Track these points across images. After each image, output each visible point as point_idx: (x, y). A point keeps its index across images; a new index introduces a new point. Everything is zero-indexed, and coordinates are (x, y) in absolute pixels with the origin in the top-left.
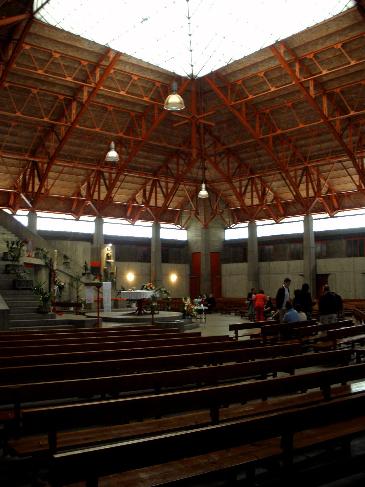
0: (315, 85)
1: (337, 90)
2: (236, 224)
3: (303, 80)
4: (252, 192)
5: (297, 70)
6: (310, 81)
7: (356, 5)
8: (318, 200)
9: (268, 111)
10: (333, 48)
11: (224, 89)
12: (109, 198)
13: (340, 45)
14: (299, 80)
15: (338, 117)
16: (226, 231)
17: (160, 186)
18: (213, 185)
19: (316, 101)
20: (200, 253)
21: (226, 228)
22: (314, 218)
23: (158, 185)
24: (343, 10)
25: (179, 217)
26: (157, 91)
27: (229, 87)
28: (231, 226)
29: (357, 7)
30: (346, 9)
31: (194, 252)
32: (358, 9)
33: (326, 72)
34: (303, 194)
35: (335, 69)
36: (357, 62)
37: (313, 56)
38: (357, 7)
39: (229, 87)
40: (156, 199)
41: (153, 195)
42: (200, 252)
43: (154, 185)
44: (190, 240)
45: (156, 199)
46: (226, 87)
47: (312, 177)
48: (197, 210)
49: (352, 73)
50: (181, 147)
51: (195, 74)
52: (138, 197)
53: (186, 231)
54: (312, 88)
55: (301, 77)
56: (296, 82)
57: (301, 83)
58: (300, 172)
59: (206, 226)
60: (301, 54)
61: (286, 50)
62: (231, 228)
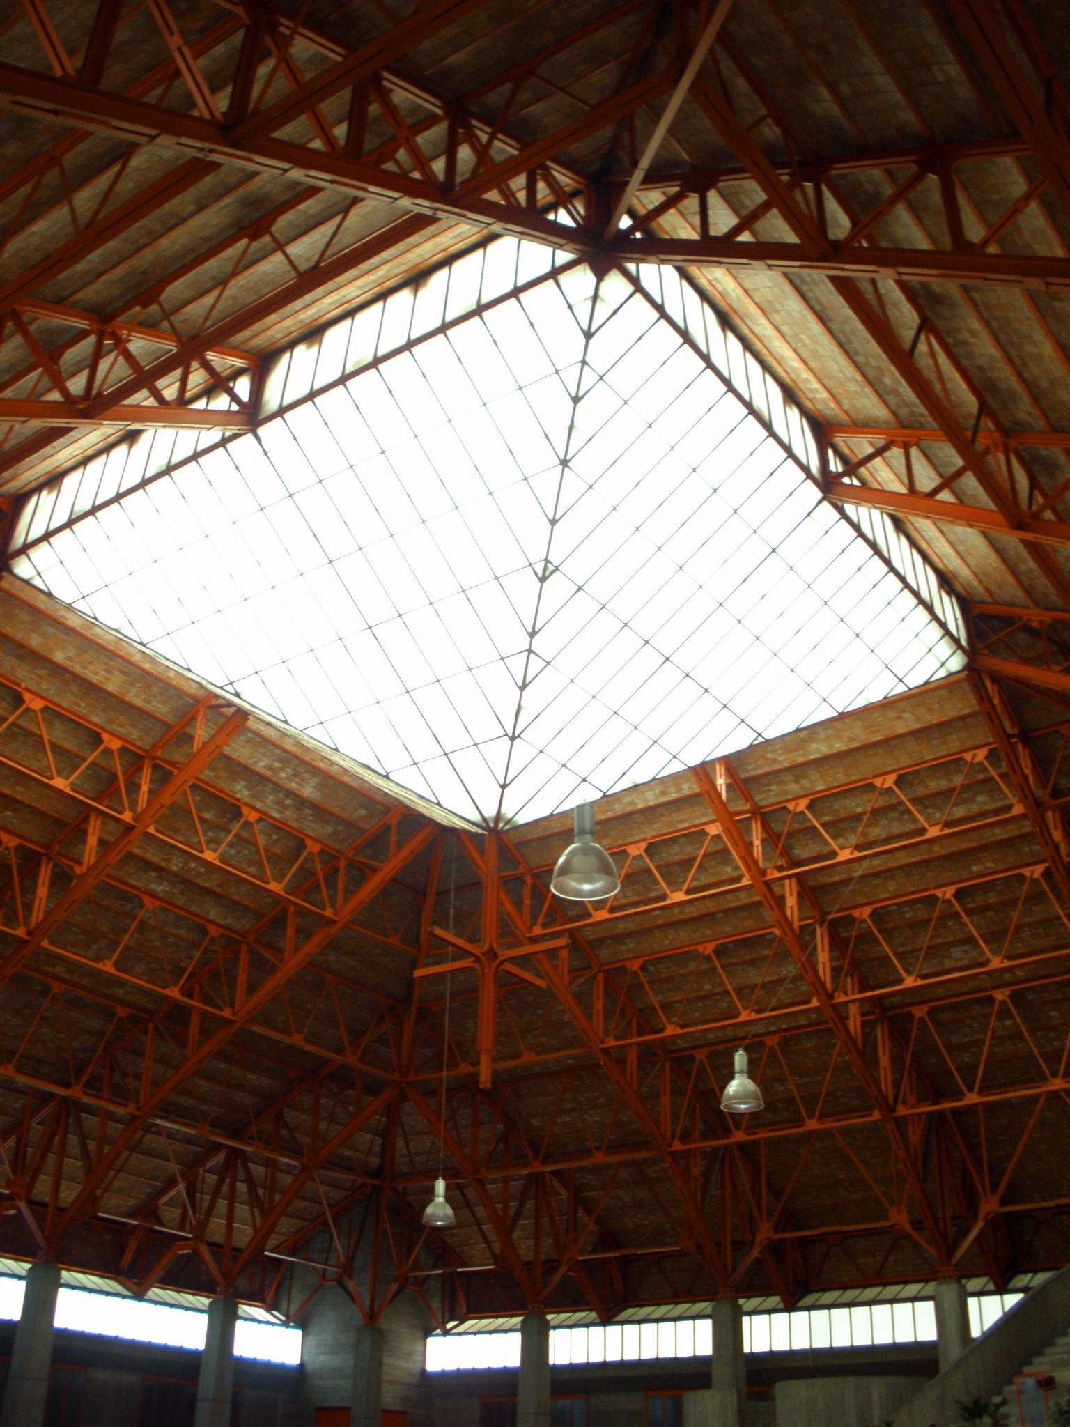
0: (800, 895)
1: (862, 912)
2: (462, 1321)
3: (777, 874)
4: (537, 1218)
5: (757, 843)
6: (787, 882)
7: (965, 668)
8: (566, 1272)
9: (635, 965)
10: (871, 786)
11: (511, 883)
12: (89, 1200)
13: (890, 781)
14: (763, 873)
15: (853, 993)
16: (431, 1341)
17: (249, 1179)
18: (405, 1188)
19: (804, 937)
20: (347, 1409)
21: (427, 1332)
22: (552, 1323)
23: (241, 1175)
24: (932, 676)
25: (277, 1287)
26: (306, 873)
27: (529, 880)
28: (449, 1326)
29: (966, 672)
30: (942, 673)
31: (327, 1405)
32: (968, 678)
33: (852, 853)
34: (525, 1248)
35: (815, 863)
36: (947, 831)
37: (896, 783)
38: (966, 672)
39: (529, 880)
40: (230, 1217)
41: (222, 1204)
42: (346, 1404)
43: (227, 1170)
44: (309, 1367)
45: (230, 1217)
46: (520, 879)
47: (554, 1204)
48: (350, 1259)
49: (694, 919)
50: (340, 1051)
51: (508, 812)
52: (164, 1204)
53: (299, 1333)
54: (791, 901)
55: (768, 865)
56: (752, 878)
57: (767, 884)
58: (516, 1186)
59: (371, 1318)
60: (768, 797)
61: (729, 781)
62: (446, 1333)
